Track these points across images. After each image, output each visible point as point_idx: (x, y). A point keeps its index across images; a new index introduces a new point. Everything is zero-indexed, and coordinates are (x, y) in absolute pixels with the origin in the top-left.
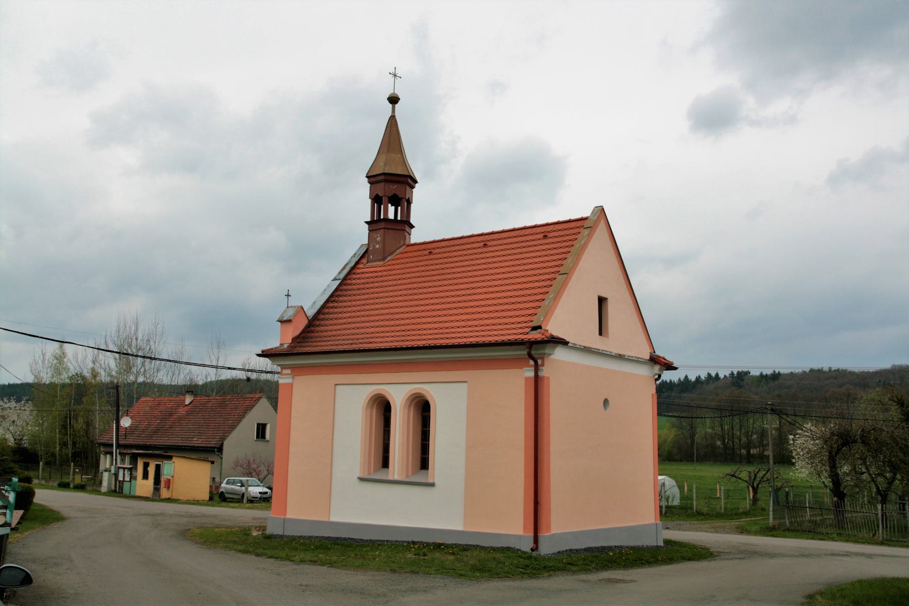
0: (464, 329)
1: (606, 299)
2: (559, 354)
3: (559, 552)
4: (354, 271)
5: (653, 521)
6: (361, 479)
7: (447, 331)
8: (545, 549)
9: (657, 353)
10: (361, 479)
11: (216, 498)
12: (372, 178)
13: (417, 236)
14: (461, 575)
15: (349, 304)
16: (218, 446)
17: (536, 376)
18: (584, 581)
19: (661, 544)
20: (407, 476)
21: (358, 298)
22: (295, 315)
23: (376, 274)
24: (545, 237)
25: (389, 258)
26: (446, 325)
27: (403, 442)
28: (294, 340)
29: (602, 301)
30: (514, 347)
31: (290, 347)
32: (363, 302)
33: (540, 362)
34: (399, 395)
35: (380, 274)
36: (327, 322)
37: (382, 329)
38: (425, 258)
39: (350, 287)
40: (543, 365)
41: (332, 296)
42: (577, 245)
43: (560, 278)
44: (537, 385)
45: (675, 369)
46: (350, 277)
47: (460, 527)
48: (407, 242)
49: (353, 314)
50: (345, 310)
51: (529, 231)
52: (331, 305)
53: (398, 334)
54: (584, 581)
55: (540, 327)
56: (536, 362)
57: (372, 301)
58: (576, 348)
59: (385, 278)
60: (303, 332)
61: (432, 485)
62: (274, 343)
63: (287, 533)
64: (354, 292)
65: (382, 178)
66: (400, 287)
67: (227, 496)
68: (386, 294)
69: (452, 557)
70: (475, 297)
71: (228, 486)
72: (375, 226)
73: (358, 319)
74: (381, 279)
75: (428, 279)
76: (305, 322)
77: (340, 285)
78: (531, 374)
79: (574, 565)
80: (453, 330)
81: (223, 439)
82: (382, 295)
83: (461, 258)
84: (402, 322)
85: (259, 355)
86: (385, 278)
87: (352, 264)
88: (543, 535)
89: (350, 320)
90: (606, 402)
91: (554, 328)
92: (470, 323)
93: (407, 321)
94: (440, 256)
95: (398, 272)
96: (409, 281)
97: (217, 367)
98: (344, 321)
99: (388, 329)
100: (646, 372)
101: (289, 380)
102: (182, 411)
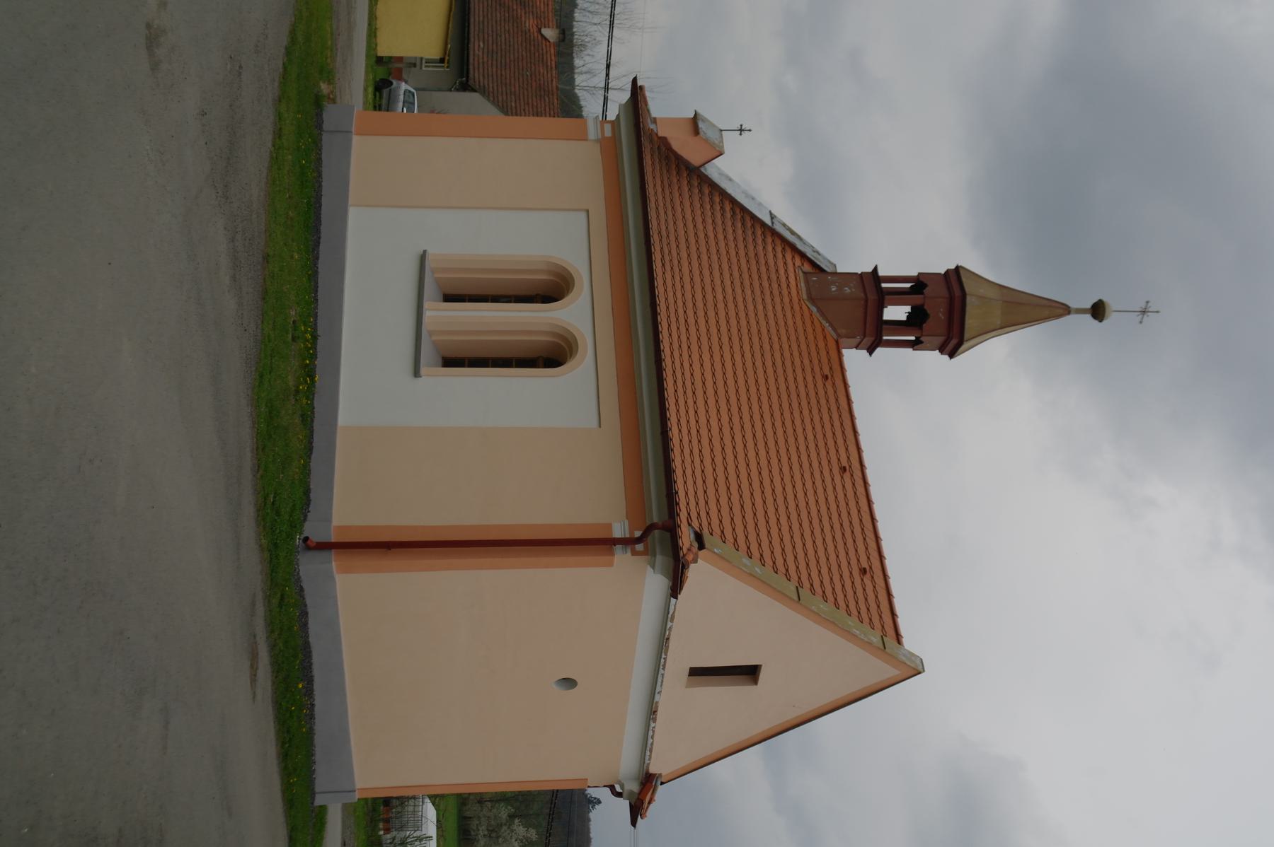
0: (693, 422)
1: (755, 682)
2: (655, 582)
3: (302, 589)
4: (788, 249)
5: (359, 785)
6: (423, 257)
7: (689, 393)
8: (309, 565)
9: (660, 789)
10: (423, 257)
11: (381, 73)
12: (955, 277)
13: (854, 358)
14: (261, 376)
15: (731, 237)
16: (471, 82)
17: (614, 542)
18: (253, 604)
19: (319, 801)
20: (431, 333)
21: (742, 253)
22: (706, 141)
23: (784, 285)
24: (863, 571)
25: (814, 309)
26: (700, 393)
27: (491, 324)
28: (664, 141)
29: (750, 673)
30: (665, 500)
31: (652, 134)
32: (734, 260)
33: (640, 547)
35: (785, 292)
36: (696, 198)
37: (688, 287)
38: (817, 369)
39: (759, 241)
40: (634, 553)
41: (744, 209)
42: (852, 622)
43: (790, 588)
44: (596, 544)
45: (634, 823)
46: (778, 242)
47: (343, 419)
48: (843, 341)
49: (712, 242)
50: (720, 230)
51: (872, 545)
52: (728, 207)
53: (681, 311)
54: (253, 604)
55: (701, 546)
56: (639, 540)
57: (736, 274)
58: (666, 617)
59: (777, 300)
60: (678, 158)
61: (417, 373)
62: (659, 108)
63: (325, 137)
64: (751, 247)
65: (957, 292)
66: (763, 323)
67: (385, 92)
68: (749, 299)
69: (291, 382)
70: (750, 445)
71: (402, 93)
73: (703, 249)
74: (776, 292)
75: (780, 371)
76: (695, 160)
77: (763, 224)
78: (618, 533)
79: (280, 605)
80: (690, 402)
81: (484, 92)
82: (748, 292)
83: (818, 428)
84: (702, 321)
85: (635, 80)
86: (777, 300)
87: (800, 246)
88: (334, 562)
89: (702, 236)
90: (569, 683)
91: (700, 572)
92: (704, 432)
93: (703, 329)
94: (821, 393)
95: (790, 322)
96: (775, 339)
97: (607, 89)
98: (700, 227)
99: (689, 296)
100: (626, 767)
101: (592, 133)
102: (530, 23)
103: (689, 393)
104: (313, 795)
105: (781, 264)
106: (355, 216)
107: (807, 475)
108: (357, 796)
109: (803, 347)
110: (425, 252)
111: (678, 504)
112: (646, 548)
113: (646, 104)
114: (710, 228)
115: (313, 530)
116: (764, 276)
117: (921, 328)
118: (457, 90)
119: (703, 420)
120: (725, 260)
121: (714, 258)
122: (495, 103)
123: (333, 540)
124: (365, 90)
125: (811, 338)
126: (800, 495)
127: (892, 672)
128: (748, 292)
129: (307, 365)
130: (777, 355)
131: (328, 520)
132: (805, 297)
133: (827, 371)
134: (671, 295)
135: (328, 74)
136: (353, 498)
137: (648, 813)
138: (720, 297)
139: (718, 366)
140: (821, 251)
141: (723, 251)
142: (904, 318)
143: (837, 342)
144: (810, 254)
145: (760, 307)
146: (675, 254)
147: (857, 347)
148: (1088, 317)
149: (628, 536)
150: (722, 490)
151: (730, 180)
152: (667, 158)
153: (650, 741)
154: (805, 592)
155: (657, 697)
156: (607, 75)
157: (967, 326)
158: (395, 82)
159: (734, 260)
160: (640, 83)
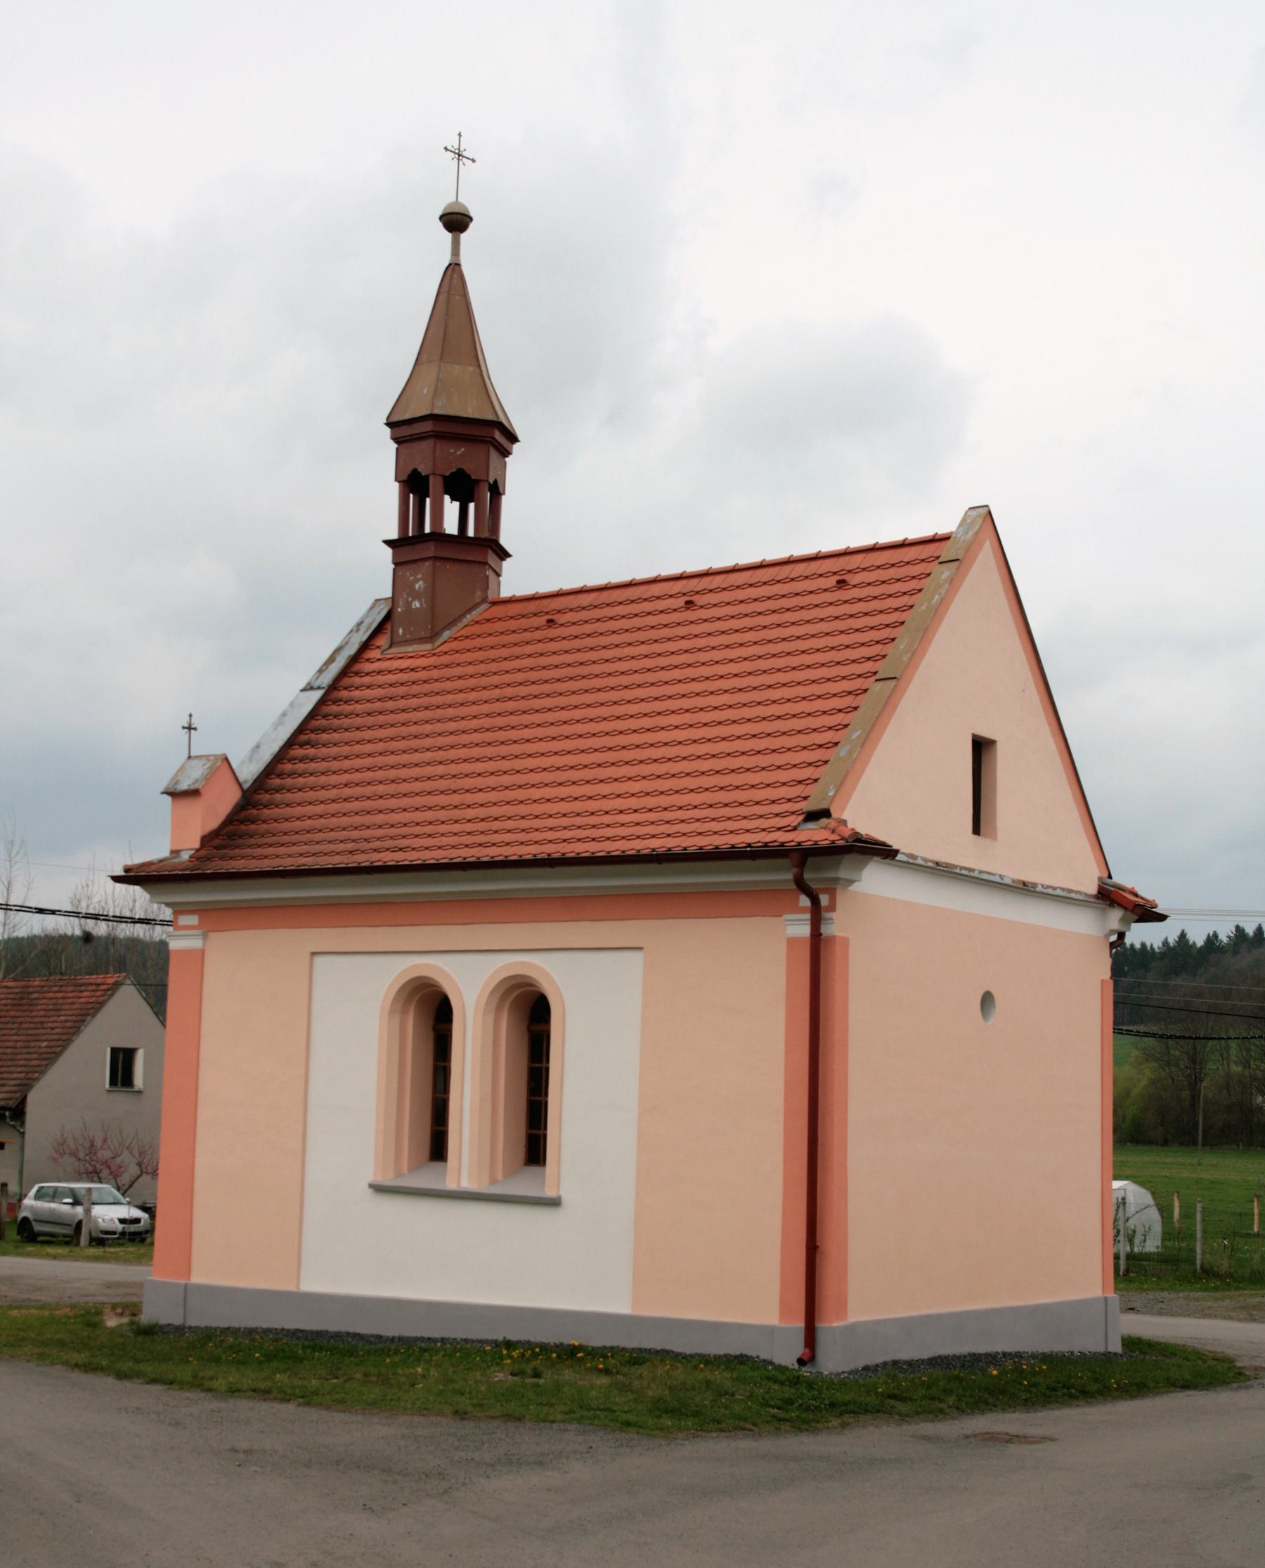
2: (873, 880)
3: (866, 1368)
6: (378, 1189)
7: (593, 820)
9: (1118, 879)
10: (378, 1189)
14: (628, 1424)
15: (346, 750)
16: (12, 1104)
17: (816, 935)
19: (1116, 1347)
24: (842, 583)
27: (477, 1091)
28: (206, 840)
29: (981, 747)
33: (824, 900)
34: (471, 981)
35: (423, 675)
37: (430, 815)
38: (538, 635)
39: (347, 708)
40: (832, 907)
47: (622, 1307)
48: (491, 595)
50: (335, 765)
52: (298, 752)
55: (826, 813)
56: (815, 901)
58: (915, 866)
60: (230, 820)
61: (555, 1203)
63: (193, 1322)
65: (427, 427)
66: (474, 709)
67: (37, 1227)
68: (439, 727)
74: (426, 688)
77: (322, 702)
78: (804, 930)
80: (607, 819)
81: (26, 1087)
85: (116, 879)
86: (436, 687)
87: (352, 650)
88: (828, 1325)
89: (347, 792)
90: (987, 1000)
91: (861, 815)
94: (574, 630)
95: (470, 670)
103: (593, 820)
104: (1108, 1357)
105: (381, 679)
106: (314, 1282)
107: (704, 657)
108: (1111, 1295)
109: (505, 652)
110: (371, 1186)
111: (766, 845)
112: (825, 891)
113: (150, 864)
114: (334, 779)
115: (787, 1354)
116: (402, 703)
117: (477, 482)
118: (23, 1123)
119: (633, 803)
120: (380, 760)
121: (380, 775)
122: (42, 1070)
123: (802, 1325)
124: (55, 1257)
125: (490, 641)
126: (733, 668)
127: (986, 553)
128: (428, 728)
129: (559, 1357)
130: (523, 691)
131: (769, 1331)
132: (428, 647)
133: (542, 620)
134: (445, 841)
135: (90, 1317)
136: (739, 1295)
137: (1149, 897)
138: (440, 770)
140: (356, 620)
141: (369, 761)
142: (456, 504)
143: (494, 603)
144: (363, 636)
145: (451, 712)
146: (380, 832)
147: (499, 575)
148: (464, 237)
149: (808, 916)
151: (258, 746)
152: (231, 836)
153: (1058, 892)
154: (883, 668)
155: (1007, 881)
156: (53, 912)
157: (477, 416)
158: (23, 1214)
159: (380, 747)
160: (120, 872)
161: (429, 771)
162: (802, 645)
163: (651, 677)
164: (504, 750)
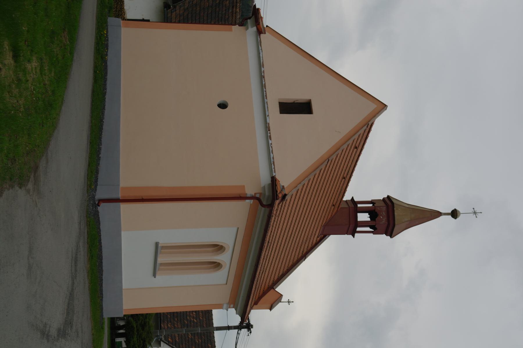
6: (157, 244)
8: (112, 20)
10: (157, 244)
12: (389, 201)
34: (224, 258)
61: (154, 275)
72: (351, 205)
93: (286, 234)
139: (292, 226)
148: (450, 216)
150: (295, 206)
157: (396, 220)
161: (309, 198)
162: (304, 211)
163: (284, 229)
164: (299, 206)
